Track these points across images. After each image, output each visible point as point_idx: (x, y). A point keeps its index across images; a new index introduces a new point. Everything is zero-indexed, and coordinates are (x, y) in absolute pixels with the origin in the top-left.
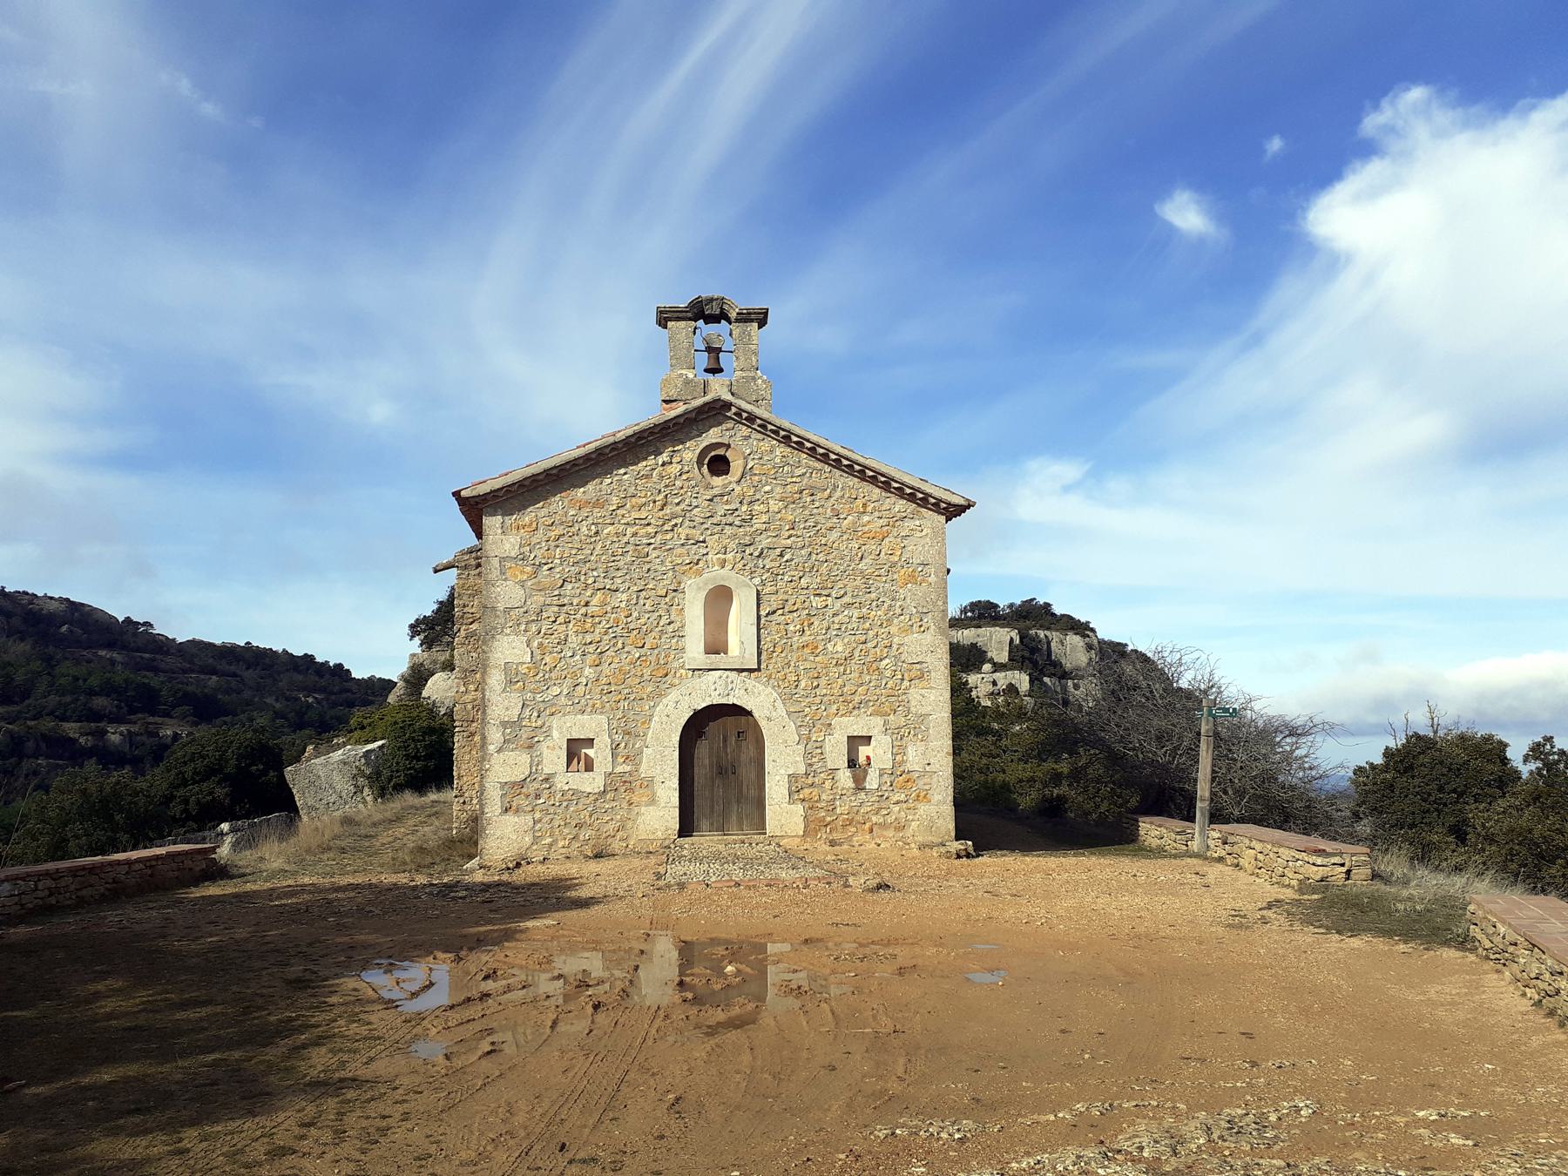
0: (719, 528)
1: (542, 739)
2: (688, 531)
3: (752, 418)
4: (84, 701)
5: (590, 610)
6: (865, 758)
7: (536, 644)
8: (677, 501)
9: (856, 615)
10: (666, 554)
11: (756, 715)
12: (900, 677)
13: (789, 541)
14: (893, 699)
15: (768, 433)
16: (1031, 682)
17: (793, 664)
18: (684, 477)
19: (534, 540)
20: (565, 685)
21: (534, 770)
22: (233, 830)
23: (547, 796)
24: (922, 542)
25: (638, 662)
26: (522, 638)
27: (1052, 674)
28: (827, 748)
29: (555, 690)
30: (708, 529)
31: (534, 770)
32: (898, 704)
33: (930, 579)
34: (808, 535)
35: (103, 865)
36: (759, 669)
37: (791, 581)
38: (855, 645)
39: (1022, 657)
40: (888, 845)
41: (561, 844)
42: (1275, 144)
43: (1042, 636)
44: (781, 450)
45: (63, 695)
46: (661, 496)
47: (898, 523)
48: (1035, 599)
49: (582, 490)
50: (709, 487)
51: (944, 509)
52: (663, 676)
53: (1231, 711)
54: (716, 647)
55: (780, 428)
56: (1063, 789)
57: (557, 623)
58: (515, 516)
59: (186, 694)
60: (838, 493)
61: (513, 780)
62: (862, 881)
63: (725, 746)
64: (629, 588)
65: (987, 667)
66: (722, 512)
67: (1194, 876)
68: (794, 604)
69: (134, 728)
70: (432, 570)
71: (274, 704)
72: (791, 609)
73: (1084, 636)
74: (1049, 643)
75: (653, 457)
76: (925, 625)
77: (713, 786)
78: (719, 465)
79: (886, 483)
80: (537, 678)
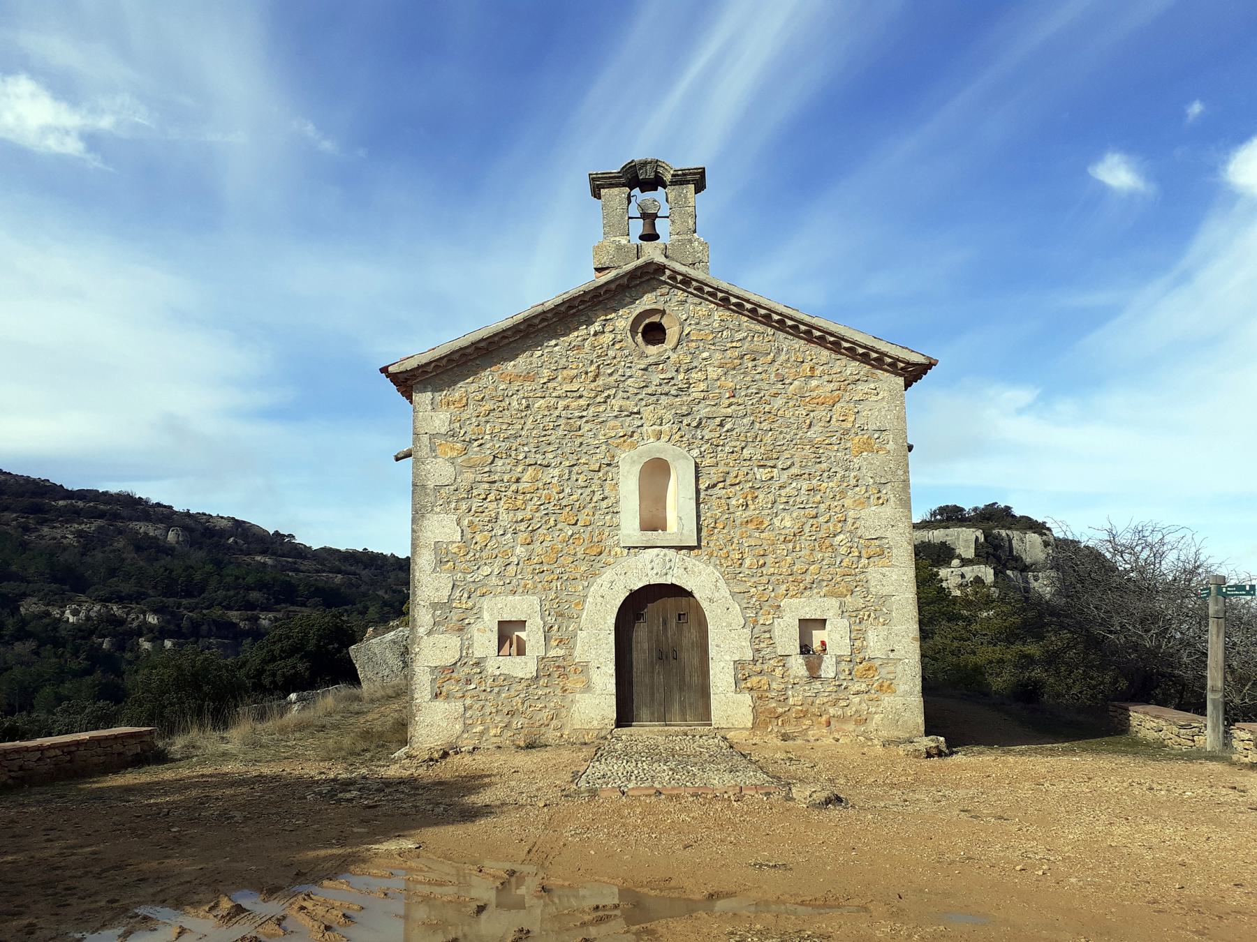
0: (654, 398)
1: (472, 621)
2: (622, 402)
3: (687, 281)
4: (243, 595)
5: (521, 486)
6: (819, 644)
7: (466, 522)
8: (609, 371)
9: (805, 487)
10: (599, 426)
11: (697, 595)
12: (857, 554)
13: (729, 410)
14: (848, 579)
15: (705, 296)
16: (996, 574)
17: (736, 541)
18: (617, 346)
19: (464, 416)
20: (495, 565)
21: (464, 654)
22: (299, 699)
23: (477, 681)
24: (879, 406)
25: (571, 541)
26: (452, 516)
27: (1014, 568)
28: (777, 632)
29: (486, 570)
30: (642, 399)
31: (464, 654)
32: (855, 584)
33: (888, 447)
34: (750, 403)
35: (5, 753)
36: (699, 547)
37: (733, 452)
38: (804, 520)
39: (987, 553)
40: (848, 741)
41: (493, 732)
42: (1196, 108)
43: (1004, 535)
44: (719, 314)
45: (228, 590)
46: (593, 368)
47: (850, 387)
48: (996, 503)
49: (512, 363)
50: (643, 355)
51: (902, 369)
52: (597, 555)
53: (1248, 588)
54: (653, 522)
55: (717, 289)
56: (1037, 673)
57: (488, 500)
58: (445, 392)
59: (317, 589)
60: (783, 357)
61: (443, 664)
62: (808, 793)
63: (665, 629)
64: (561, 463)
65: (956, 562)
66: (657, 382)
67: (1231, 791)
68: (736, 477)
69: (279, 615)
70: (393, 458)
71: (384, 596)
72: (733, 482)
73: (1042, 534)
74: (1010, 541)
75: (585, 327)
76: (884, 497)
77: (653, 672)
78: (654, 333)
79: (835, 344)
80: (468, 557)
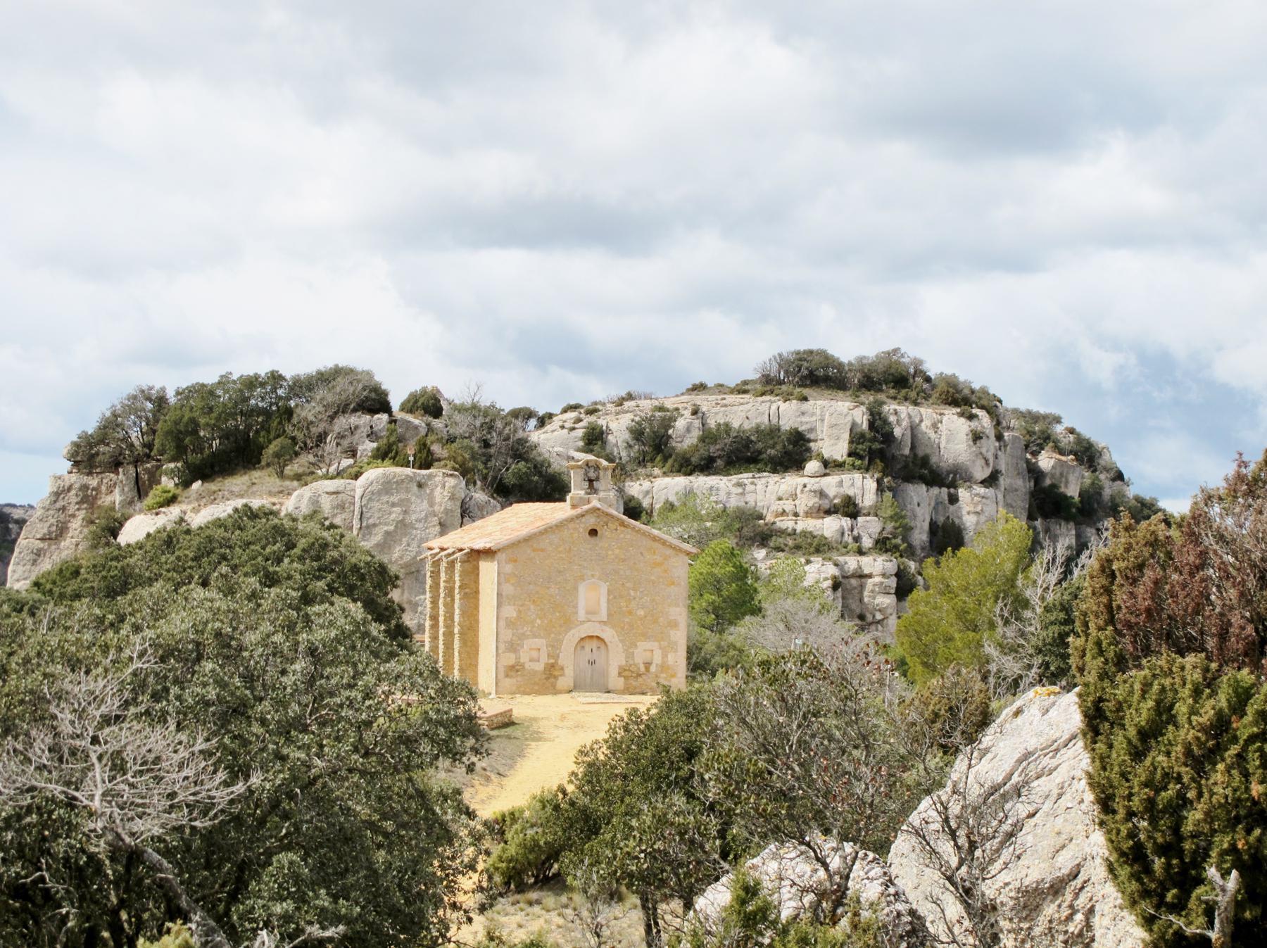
16: (880, 489)
65: (812, 466)
